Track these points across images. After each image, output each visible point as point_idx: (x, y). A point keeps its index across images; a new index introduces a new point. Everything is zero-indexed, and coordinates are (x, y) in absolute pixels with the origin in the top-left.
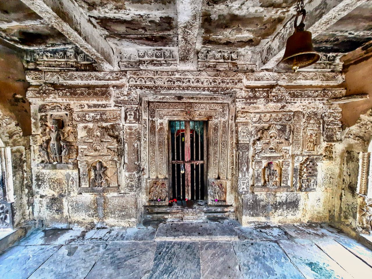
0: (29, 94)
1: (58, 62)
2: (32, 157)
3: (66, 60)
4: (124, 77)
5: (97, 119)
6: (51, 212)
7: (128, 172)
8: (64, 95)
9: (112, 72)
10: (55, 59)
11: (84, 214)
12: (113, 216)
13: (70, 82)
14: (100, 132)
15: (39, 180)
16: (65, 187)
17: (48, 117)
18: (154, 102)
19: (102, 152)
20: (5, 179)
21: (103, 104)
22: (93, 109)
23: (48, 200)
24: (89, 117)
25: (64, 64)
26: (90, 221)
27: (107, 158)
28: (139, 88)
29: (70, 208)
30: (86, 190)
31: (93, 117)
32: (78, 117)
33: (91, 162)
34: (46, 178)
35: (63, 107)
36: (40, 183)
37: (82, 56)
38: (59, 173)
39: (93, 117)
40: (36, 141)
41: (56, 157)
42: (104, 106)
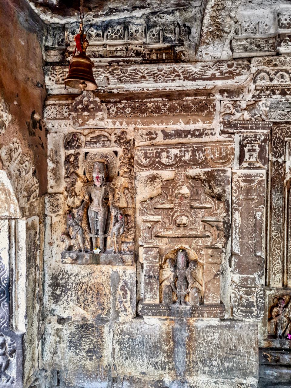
0: (50, 112)
1: (110, 46)
2: (47, 239)
3: (125, 41)
4: (245, 71)
5: (185, 162)
6: (78, 355)
7: (241, 272)
8: (120, 114)
9: (219, 62)
10: (105, 41)
11: (145, 363)
12: (207, 369)
13: (132, 87)
14: (191, 188)
15: (58, 285)
16: (108, 301)
17: (81, 157)
18: (282, 123)
19: (191, 229)
20: (12, 283)
21: (195, 130)
22: (175, 141)
23: (74, 329)
24: (168, 157)
25: (121, 50)
26: (157, 379)
27: (203, 242)
28: (277, 92)
29: (117, 347)
30: (153, 310)
31: (176, 156)
32: (146, 157)
33: (166, 249)
34: (70, 281)
35: (113, 138)
36: (58, 292)
37: (154, 33)
38: (97, 273)
39: (176, 156)
40: (57, 206)
41: (96, 239)
42: (197, 133)
